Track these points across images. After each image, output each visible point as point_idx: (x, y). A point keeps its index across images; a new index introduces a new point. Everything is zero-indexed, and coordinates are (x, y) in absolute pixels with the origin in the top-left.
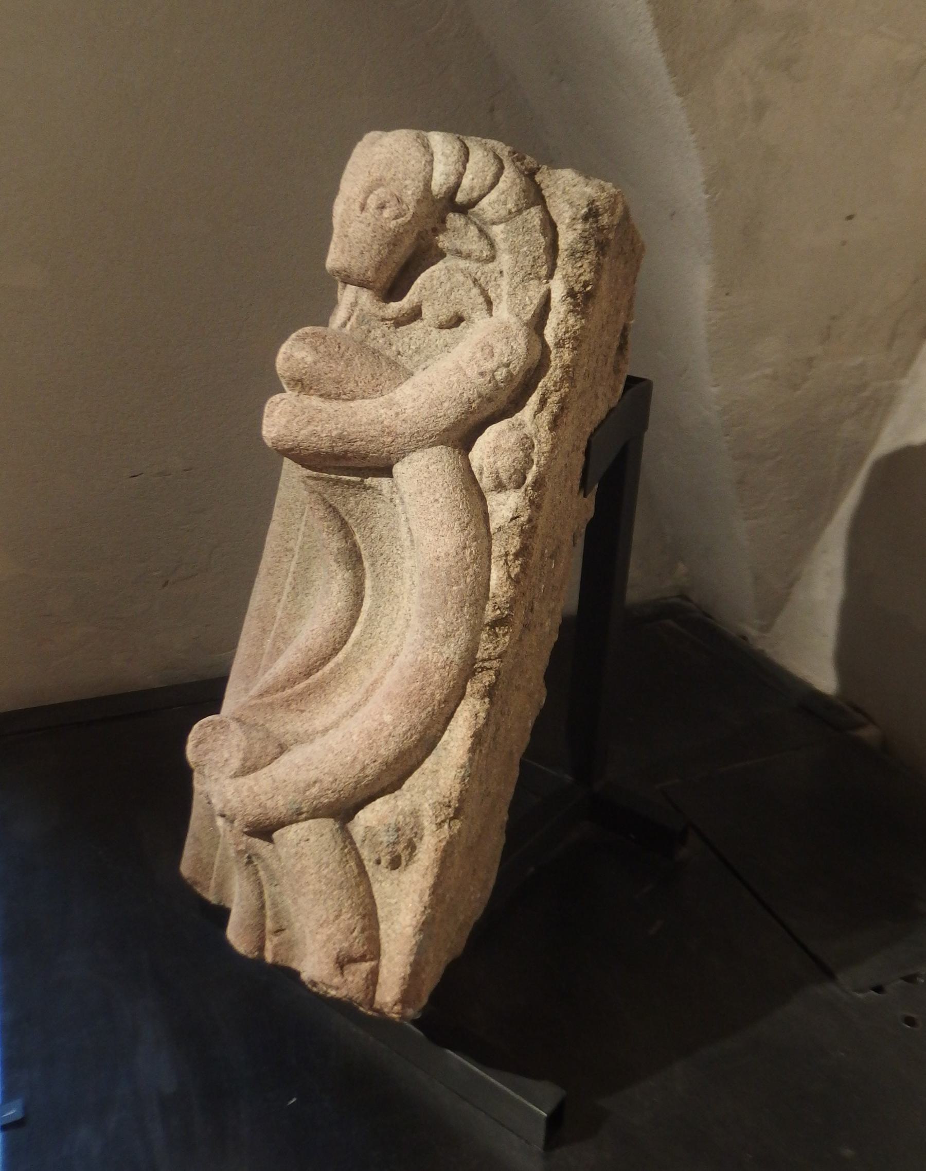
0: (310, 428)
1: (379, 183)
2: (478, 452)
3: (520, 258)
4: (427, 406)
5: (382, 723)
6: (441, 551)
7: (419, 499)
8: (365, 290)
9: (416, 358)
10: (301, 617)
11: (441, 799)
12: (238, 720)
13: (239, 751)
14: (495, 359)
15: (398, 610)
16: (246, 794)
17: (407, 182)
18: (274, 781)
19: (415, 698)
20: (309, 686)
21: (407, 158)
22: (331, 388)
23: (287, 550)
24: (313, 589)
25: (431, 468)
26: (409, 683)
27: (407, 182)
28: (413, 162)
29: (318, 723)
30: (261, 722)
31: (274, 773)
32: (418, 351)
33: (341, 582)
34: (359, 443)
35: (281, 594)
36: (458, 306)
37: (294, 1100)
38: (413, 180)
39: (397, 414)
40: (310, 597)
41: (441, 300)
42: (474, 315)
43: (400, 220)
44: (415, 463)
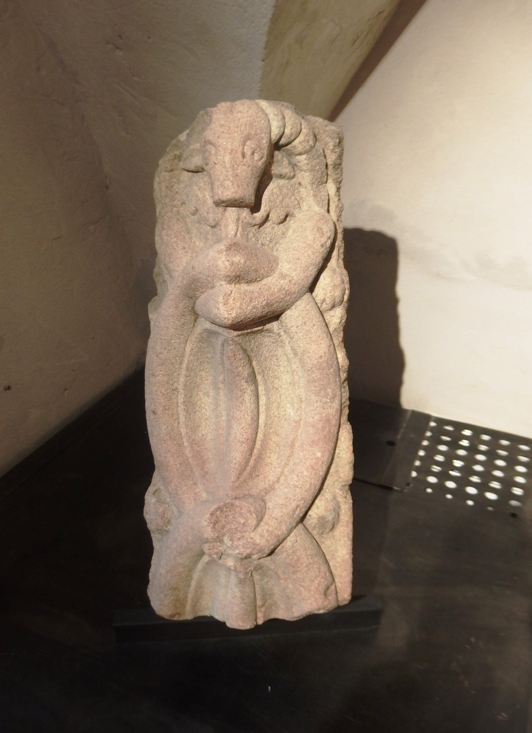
0: (252, 304)
1: (248, 137)
2: (321, 290)
3: (316, 174)
4: (302, 272)
5: (317, 459)
6: (321, 352)
7: (304, 327)
8: (245, 209)
9: (271, 245)
10: (198, 427)
11: (343, 483)
12: (236, 498)
13: (251, 514)
14: (325, 235)
15: (280, 396)
16: (266, 535)
17: (263, 135)
18: (277, 519)
19: (328, 437)
20: (255, 460)
21: (259, 119)
22: (253, 276)
23: (174, 390)
24: (198, 407)
25: (307, 308)
26: (323, 431)
27: (263, 135)
28: (263, 121)
29: (272, 477)
30: (247, 493)
31: (273, 515)
32: (271, 241)
33: (251, 393)
34: (275, 305)
35: (178, 418)
36: (288, 209)
37: (269, 688)
38: (265, 133)
39: (290, 281)
40: (197, 413)
41: (280, 207)
42: (295, 212)
43: (263, 159)
44: (299, 308)
